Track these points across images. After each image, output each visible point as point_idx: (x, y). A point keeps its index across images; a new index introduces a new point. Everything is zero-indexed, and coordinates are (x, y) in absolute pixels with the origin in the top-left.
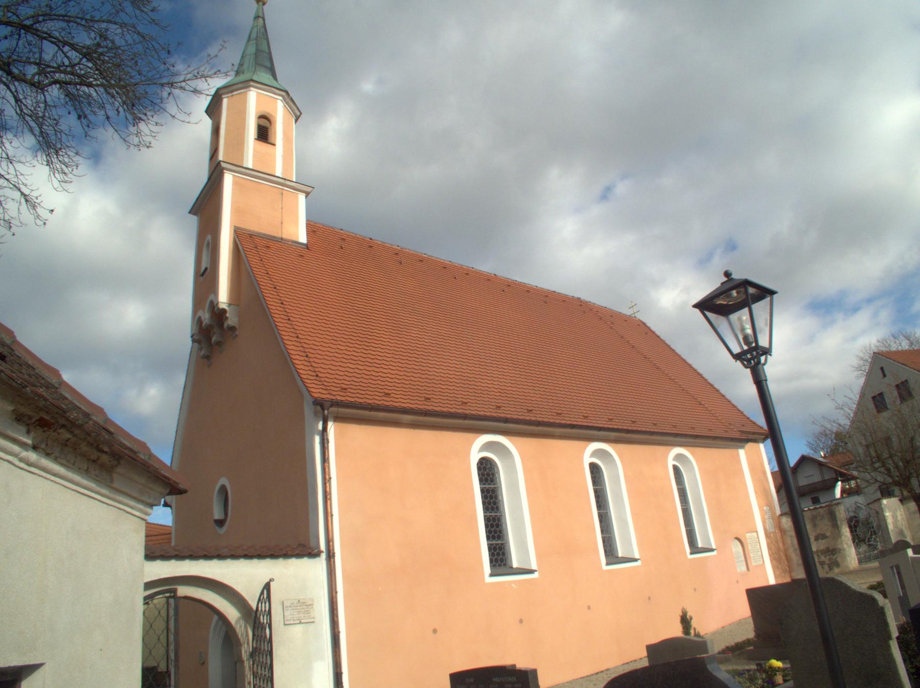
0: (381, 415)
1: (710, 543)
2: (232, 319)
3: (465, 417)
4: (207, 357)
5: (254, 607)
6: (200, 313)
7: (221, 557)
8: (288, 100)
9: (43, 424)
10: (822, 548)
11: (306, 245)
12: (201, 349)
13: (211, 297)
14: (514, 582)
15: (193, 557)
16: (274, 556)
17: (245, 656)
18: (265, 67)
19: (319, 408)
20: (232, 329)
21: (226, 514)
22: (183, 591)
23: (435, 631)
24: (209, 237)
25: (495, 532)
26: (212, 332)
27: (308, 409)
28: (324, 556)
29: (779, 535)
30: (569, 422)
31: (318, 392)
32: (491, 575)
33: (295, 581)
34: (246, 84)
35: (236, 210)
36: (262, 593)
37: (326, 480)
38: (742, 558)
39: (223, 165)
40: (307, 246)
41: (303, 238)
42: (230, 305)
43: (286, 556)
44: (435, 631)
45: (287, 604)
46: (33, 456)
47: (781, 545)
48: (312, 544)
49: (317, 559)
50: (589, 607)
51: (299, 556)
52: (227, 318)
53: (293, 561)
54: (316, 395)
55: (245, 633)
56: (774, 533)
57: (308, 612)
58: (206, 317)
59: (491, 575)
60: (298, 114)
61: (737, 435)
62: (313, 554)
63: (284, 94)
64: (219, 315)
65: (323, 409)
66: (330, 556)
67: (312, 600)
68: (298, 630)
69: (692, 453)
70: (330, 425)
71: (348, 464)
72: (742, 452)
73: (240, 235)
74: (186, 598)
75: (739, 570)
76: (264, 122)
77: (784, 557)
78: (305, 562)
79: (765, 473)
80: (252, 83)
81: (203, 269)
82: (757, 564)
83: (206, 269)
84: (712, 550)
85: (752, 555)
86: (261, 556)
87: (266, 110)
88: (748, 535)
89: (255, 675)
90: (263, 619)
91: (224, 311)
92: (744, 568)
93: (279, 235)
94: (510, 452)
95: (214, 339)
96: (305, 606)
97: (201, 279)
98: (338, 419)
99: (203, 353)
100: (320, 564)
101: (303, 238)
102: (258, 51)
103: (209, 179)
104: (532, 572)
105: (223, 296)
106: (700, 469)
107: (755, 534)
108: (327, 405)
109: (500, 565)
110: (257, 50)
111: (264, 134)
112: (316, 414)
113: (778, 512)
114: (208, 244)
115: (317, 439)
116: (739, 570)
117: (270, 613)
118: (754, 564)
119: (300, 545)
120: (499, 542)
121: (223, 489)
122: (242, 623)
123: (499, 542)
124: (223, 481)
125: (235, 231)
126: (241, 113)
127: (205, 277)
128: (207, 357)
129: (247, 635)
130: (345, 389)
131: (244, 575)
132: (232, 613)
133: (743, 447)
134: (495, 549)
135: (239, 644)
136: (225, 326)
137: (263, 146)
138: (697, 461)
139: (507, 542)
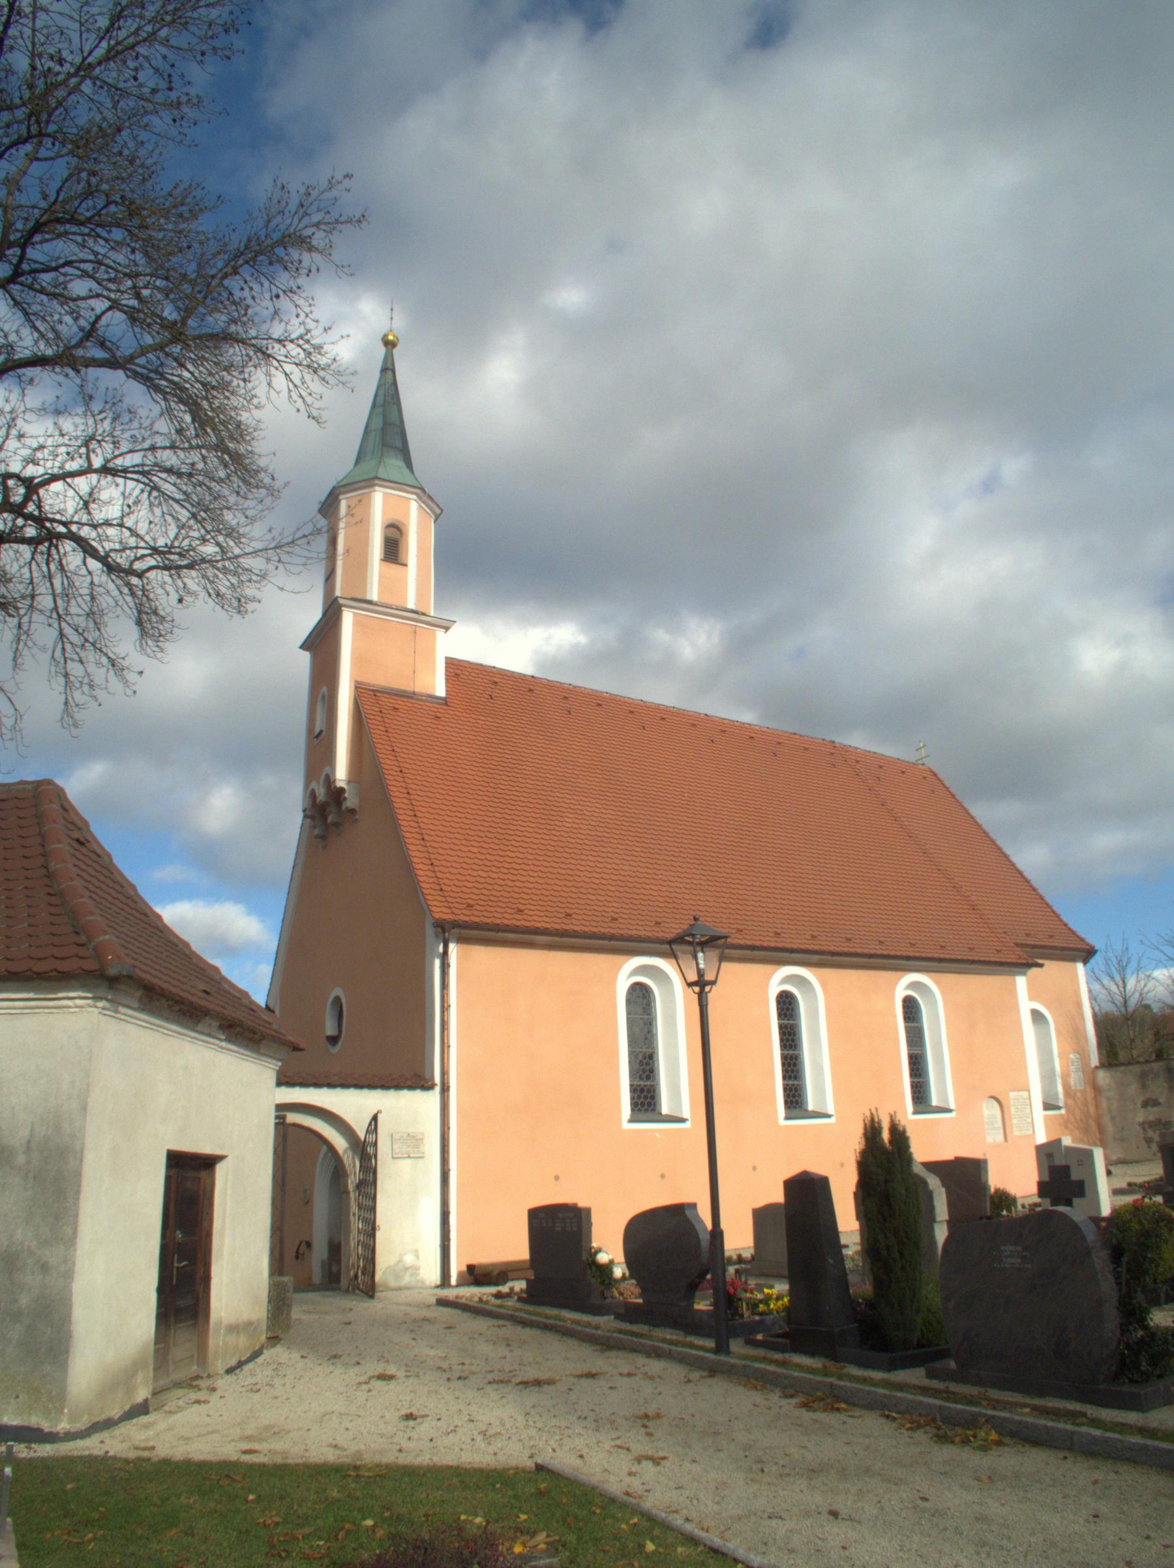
0: (511, 936)
1: (946, 1100)
2: (351, 801)
3: (612, 938)
4: (323, 837)
5: (362, 1136)
6: (314, 785)
7: (331, 1085)
8: (425, 498)
9: (230, 1026)
10: (1151, 1118)
11: (445, 699)
12: (314, 827)
13: (327, 770)
14: (659, 1131)
15: (304, 1084)
16: (385, 1087)
17: (351, 1186)
18: (396, 448)
19: (440, 930)
20: (352, 811)
21: (340, 1031)
22: (292, 1118)
23: (557, 1178)
24: (324, 689)
25: (789, 1065)
26: (326, 813)
27: (430, 930)
28: (438, 1089)
29: (1090, 1094)
30: (749, 943)
31: (441, 912)
32: (631, 1121)
33: (405, 1113)
34: (370, 482)
35: (357, 659)
36: (370, 1124)
37: (445, 1008)
38: (1000, 1124)
39: (341, 601)
40: (445, 701)
41: (440, 691)
42: (349, 782)
43: (398, 1087)
44: (557, 1178)
45: (396, 1137)
46: (224, 1044)
47: (1092, 1110)
48: (427, 1076)
49: (430, 1092)
50: (754, 1168)
51: (411, 1087)
52: (345, 799)
53: (405, 1093)
54: (437, 916)
55: (352, 1164)
56: (1083, 1092)
57: (418, 1147)
58: (321, 794)
59: (631, 1121)
60: (438, 511)
61: (1012, 958)
62: (427, 1086)
63: (418, 491)
64: (337, 794)
65: (444, 932)
66: (445, 1089)
67: (423, 1134)
68: (406, 1164)
69: (938, 983)
70: (453, 948)
71: (470, 987)
72: (1021, 982)
73: (362, 692)
74: (295, 1125)
75: (989, 1139)
76: (393, 533)
77: (1094, 1127)
78: (418, 1095)
79: (1079, 1005)
80: (377, 482)
81: (317, 731)
82: (1024, 1133)
83: (321, 731)
84: (949, 1111)
85: (1014, 1121)
86: (371, 1086)
87: (395, 516)
88: (1012, 1095)
89: (360, 1207)
90: (370, 1150)
91: (342, 790)
92: (1000, 1138)
93: (409, 689)
94: (668, 977)
95: (330, 819)
96: (415, 1140)
97: (316, 741)
98: (461, 940)
99: (317, 832)
100: (434, 1096)
101: (440, 691)
102: (386, 424)
103: (324, 615)
104: (683, 1120)
105: (341, 772)
106: (945, 1003)
107: (1025, 1094)
108: (447, 927)
109: (646, 1110)
110: (385, 423)
111: (393, 550)
112: (437, 936)
113: (1094, 1060)
114: (324, 697)
115: (437, 963)
116: (989, 1139)
117: (375, 1144)
118: (1016, 1133)
119: (415, 1075)
120: (648, 1083)
121: (337, 1001)
122: (350, 1153)
123: (648, 1083)
124: (338, 992)
125: (356, 688)
126: (363, 523)
127: (320, 743)
128: (323, 837)
129: (354, 1166)
130: (471, 906)
131: (353, 1105)
132: (340, 1143)
133: (1024, 974)
134: (791, 1090)
135: (346, 1175)
136: (344, 807)
137: (393, 569)
138: (942, 992)
139: (658, 1084)
